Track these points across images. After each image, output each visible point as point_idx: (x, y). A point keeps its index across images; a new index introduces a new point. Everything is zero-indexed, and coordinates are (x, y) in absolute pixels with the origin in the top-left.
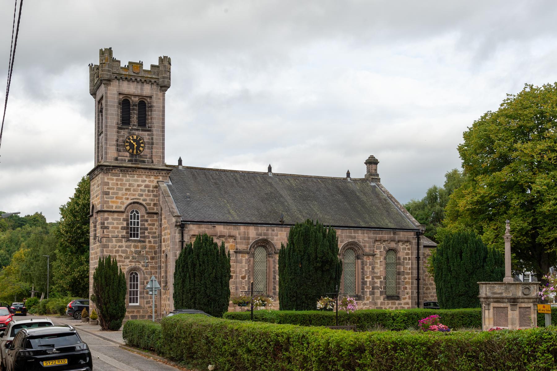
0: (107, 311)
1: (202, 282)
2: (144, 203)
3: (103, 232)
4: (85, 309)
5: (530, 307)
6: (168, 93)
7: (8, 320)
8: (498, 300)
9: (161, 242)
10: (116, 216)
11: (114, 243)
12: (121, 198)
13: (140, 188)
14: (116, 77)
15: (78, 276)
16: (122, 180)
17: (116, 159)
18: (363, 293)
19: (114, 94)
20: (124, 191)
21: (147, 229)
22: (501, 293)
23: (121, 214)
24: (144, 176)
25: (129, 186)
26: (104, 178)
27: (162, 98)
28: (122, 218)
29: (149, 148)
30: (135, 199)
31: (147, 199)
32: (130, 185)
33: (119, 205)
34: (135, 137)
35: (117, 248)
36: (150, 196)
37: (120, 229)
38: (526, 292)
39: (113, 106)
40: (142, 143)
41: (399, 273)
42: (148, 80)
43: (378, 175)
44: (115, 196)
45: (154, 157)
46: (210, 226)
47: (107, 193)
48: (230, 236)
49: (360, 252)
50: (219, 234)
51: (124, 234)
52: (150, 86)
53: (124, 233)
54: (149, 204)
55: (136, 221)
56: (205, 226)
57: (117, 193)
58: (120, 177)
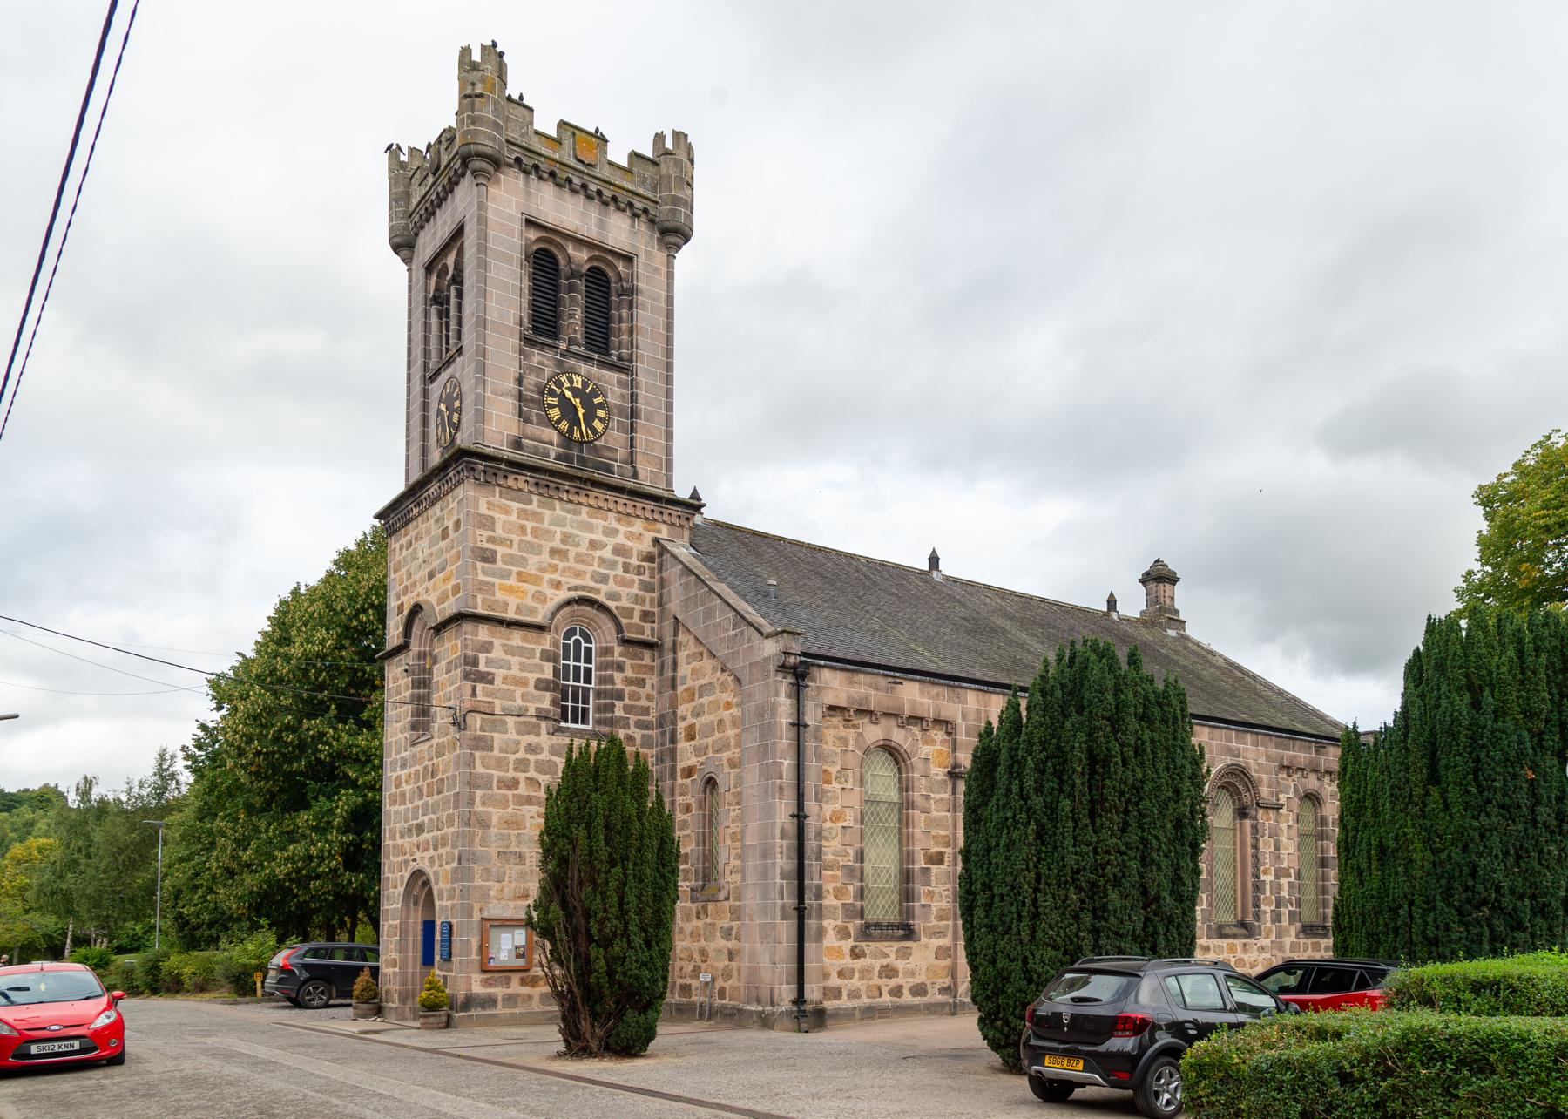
0: (610, 973)
1: (1134, 837)
2: (612, 605)
3: (474, 694)
4: (367, 972)
7: (103, 1021)
9: (673, 740)
10: (517, 638)
11: (512, 735)
12: (536, 580)
13: (598, 553)
14: (518, 160)
15: (288, 874)
16: (537, 517)
17: (517, 444)
18: (1257, 916)
19: (510, 218)
20: (545, 557)
21: (620, 695)
23: (534, 634)
24: (612, 516)
25: (563, 541)
26: (476, 500)
27: (664, 270)
28: (538, 649)
29: (621, 427)
30: (584, 588)
31: (623, 593)
32: (566, 538)
33: (529, 602)
35: (521, 754)
36: (630, 584)
37: (531, 688)
39: (509, 259)
40: (601, 406)
42: (623, 198)
43: (1177, 612)
44: (515, 569)
45: (639, 459)
46: (883, 682)
47: (488, 557)
48: (939, 722)
49: (1247, 798)
50: (907, 712)
51: (546, 704)
52: (628, 221)
53: (545, 701)
54: (629, 613)
55: (582, 665)
56: (869, 678)
57: (522, 561)
58: (534, 507)
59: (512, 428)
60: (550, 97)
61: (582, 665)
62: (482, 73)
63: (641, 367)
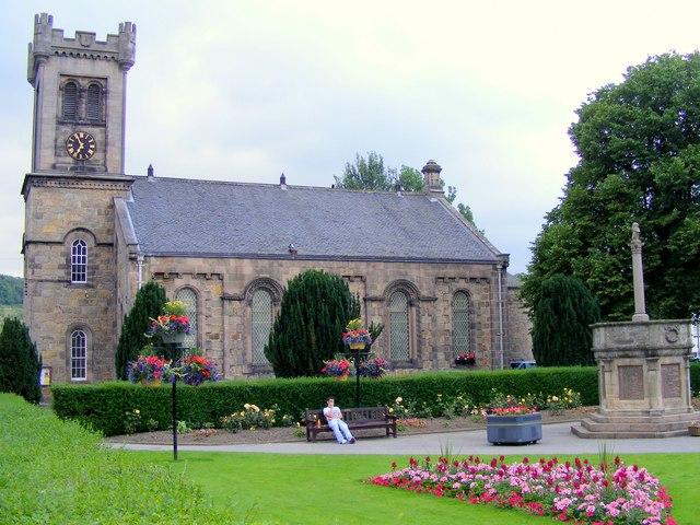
5: (678, 364)
6: (131, 73)
8: (626, 353)
17: (54, 167)
22: (631, 341)
31: (97, 223)
34: (82, 136)
38: (672, 337)
41: (472, 326)
59: (52, 160)
60: (69, 25)
61: (81, 256)
62: (43, 23)
63: (109, 124)
